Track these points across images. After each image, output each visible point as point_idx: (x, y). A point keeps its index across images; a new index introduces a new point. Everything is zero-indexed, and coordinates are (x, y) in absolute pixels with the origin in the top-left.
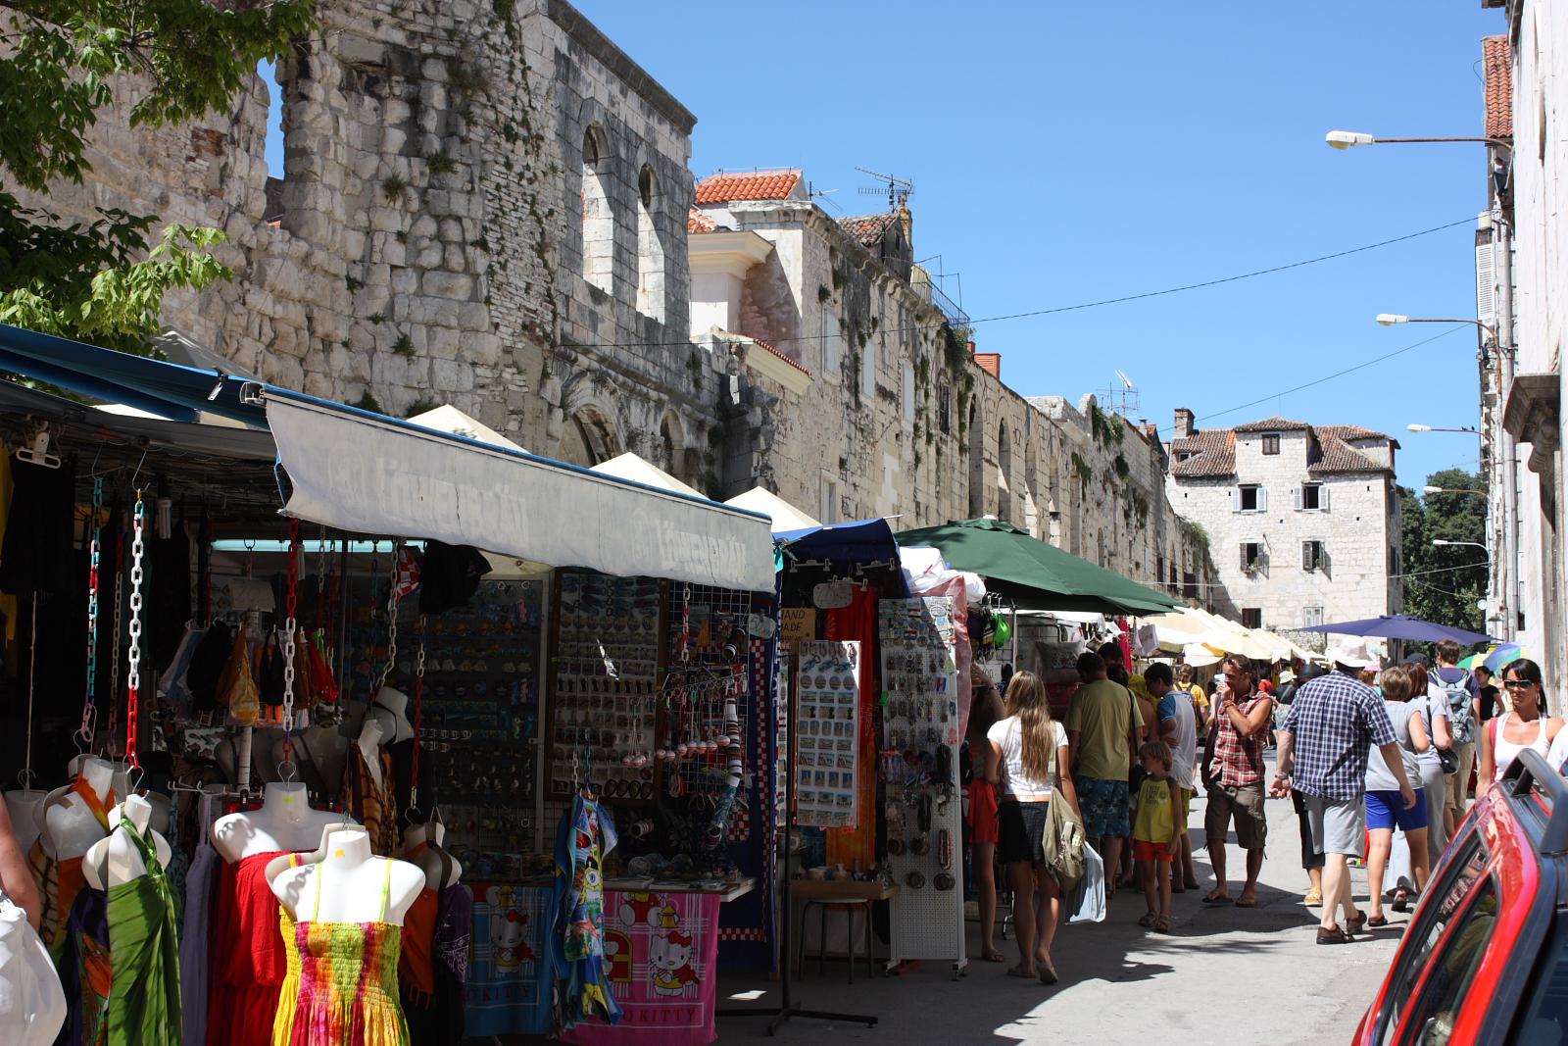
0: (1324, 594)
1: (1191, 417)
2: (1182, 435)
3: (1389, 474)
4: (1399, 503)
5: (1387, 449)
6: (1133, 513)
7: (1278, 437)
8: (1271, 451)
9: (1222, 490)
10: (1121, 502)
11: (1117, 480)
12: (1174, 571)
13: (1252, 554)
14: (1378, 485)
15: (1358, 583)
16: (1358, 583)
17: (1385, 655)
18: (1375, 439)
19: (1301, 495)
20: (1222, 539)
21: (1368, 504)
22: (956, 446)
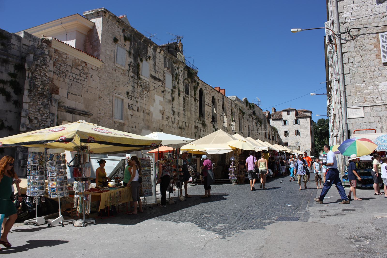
0: (299, 140)
1: (275, 109)
2: (273, 112)
3: (310, 117)
4: (313, 124)
5: (310, 113)
6: (258, 123)
8: (289, 114)
9: (280, 121)
10: (254, 121)
11: (253, 116)
12: (269, 136)
13: (286, 133)
14: (309, 119)
15: (305, 137)
16: (305, 137)
17: (311, 150)
18: (308, 112)
19: (294, 122)
20: (280, 130)
21: (307, 123)
22: (193, 99)
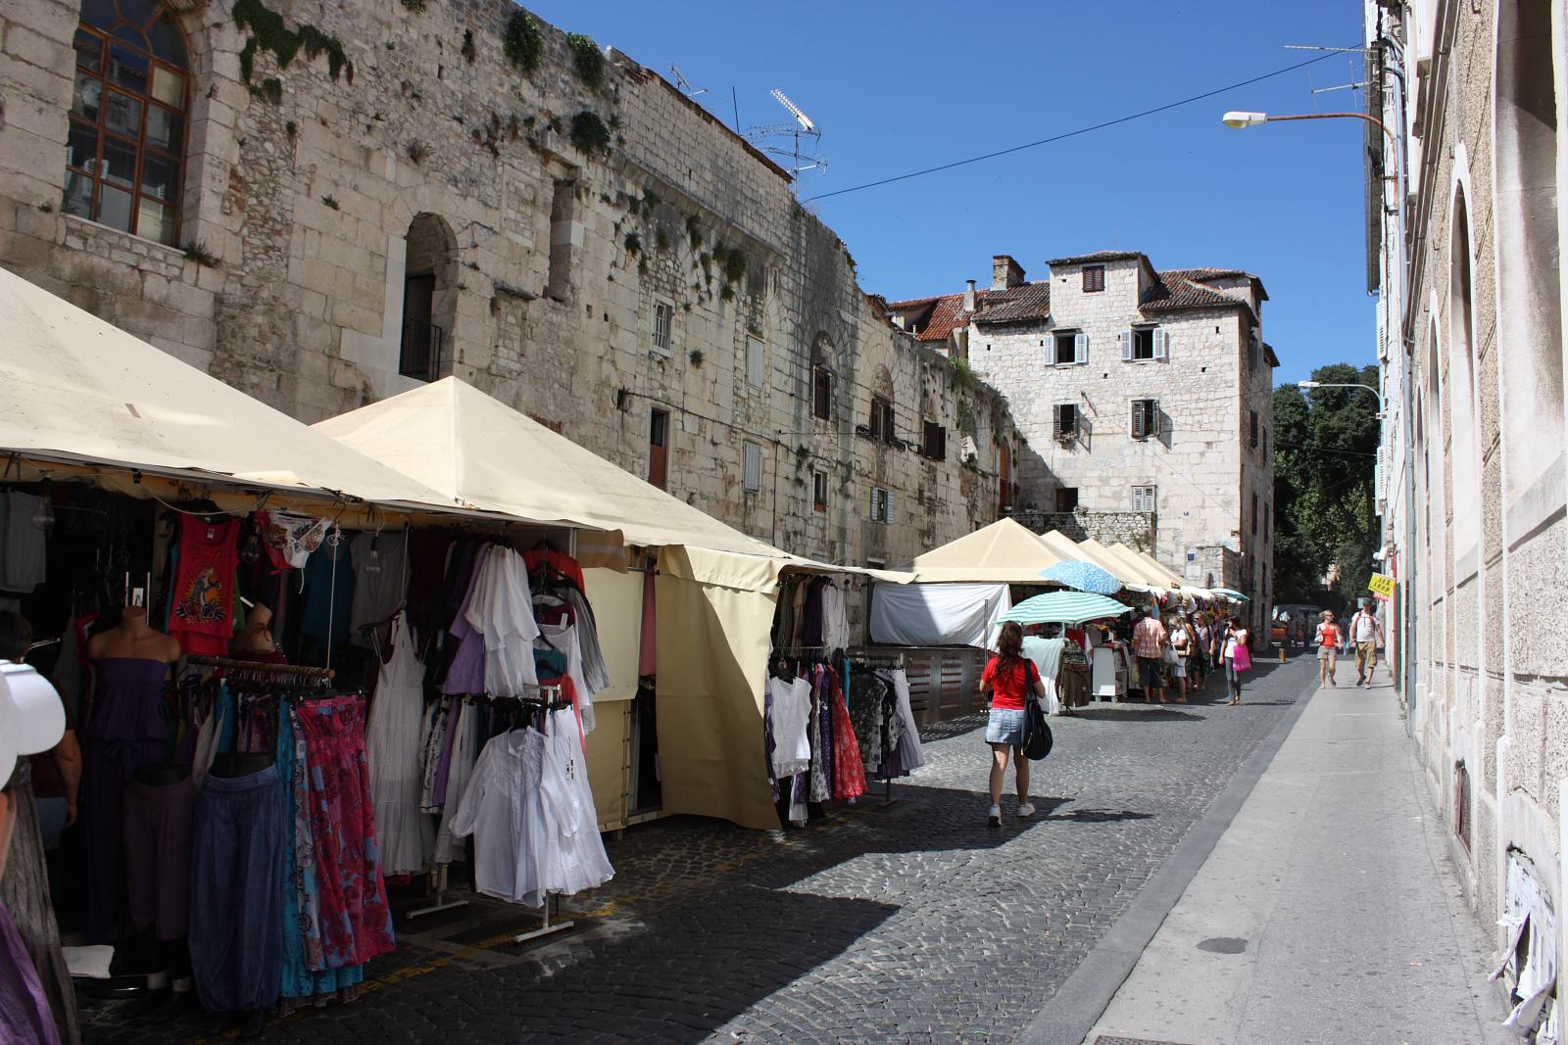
7: (1102, 268)
9: (1033, 338)
13: (1068, 421)
14: (1231, 324)
15: (1202, 454)
16: (1202, 454)
18: (1234, 278)
20: (1031, 401)
21: (1217, 351)
